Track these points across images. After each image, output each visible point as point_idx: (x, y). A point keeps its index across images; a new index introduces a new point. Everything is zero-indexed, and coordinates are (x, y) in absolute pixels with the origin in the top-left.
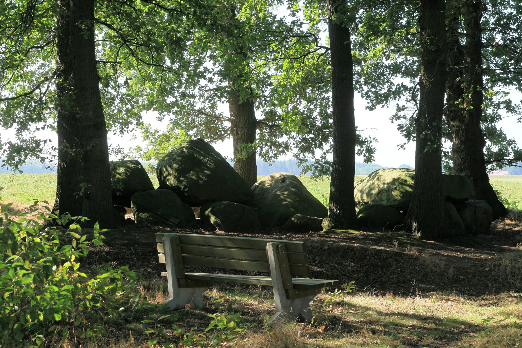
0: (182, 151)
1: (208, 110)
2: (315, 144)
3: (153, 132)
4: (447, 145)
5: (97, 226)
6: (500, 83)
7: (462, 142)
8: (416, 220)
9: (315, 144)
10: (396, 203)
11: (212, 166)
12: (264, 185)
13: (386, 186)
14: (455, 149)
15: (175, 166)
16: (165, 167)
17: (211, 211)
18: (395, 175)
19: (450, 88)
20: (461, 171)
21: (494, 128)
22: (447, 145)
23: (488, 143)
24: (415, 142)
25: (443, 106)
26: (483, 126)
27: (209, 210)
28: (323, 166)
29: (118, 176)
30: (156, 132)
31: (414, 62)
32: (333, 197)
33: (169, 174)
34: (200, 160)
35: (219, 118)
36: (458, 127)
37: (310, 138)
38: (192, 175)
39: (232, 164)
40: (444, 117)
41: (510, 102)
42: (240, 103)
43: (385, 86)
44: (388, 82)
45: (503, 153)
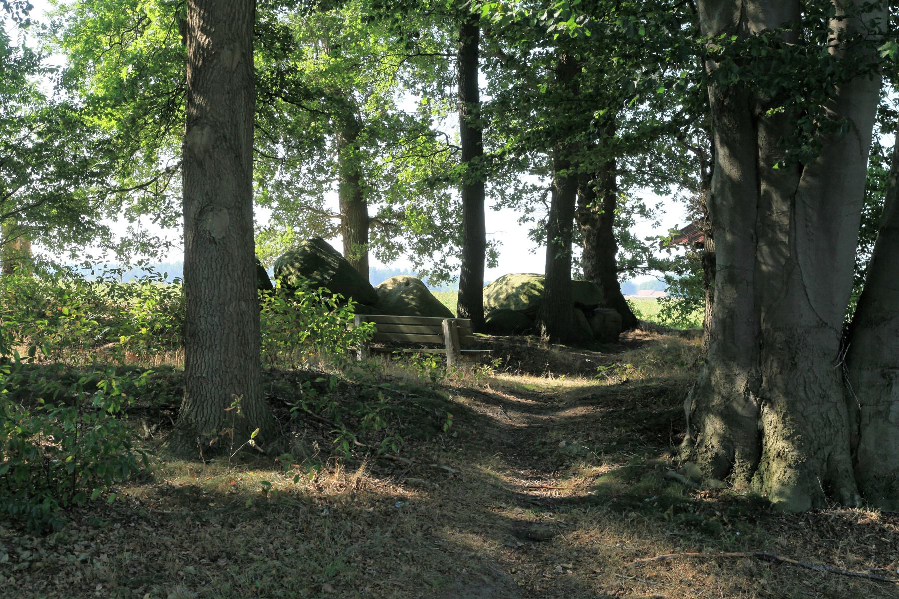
0: (304, 250)
1: (314, 204)
2: (433, 246)
4: (577, 251)
5: (350, 300)
6: (635, 185)
7: (593, 248)
8: (545, 324)
9: (433, 246)
10: (525, 308)
11: (336, 266)
14: (585, 256)
15: (297, 264)
16: (286, 266)
18: (525, 279)
19: (583, 190)
20: (592, 278)
21: (628, 234)
22: (577, 251)
23: (621, 249)
24: (546, 247)
25: (574, 207)
26: (616, 231)
28: (441, 271)
31: (544, 158)
32: (462, 300)
33: (290, 273)
34: (323, 259)
35: (326, 214)
36: (589, 231)
37: (428, 239)
40: (574, 220)
41: (644, 206)
43: (512, 184)
44: (515, 179)
45: (637, 260)
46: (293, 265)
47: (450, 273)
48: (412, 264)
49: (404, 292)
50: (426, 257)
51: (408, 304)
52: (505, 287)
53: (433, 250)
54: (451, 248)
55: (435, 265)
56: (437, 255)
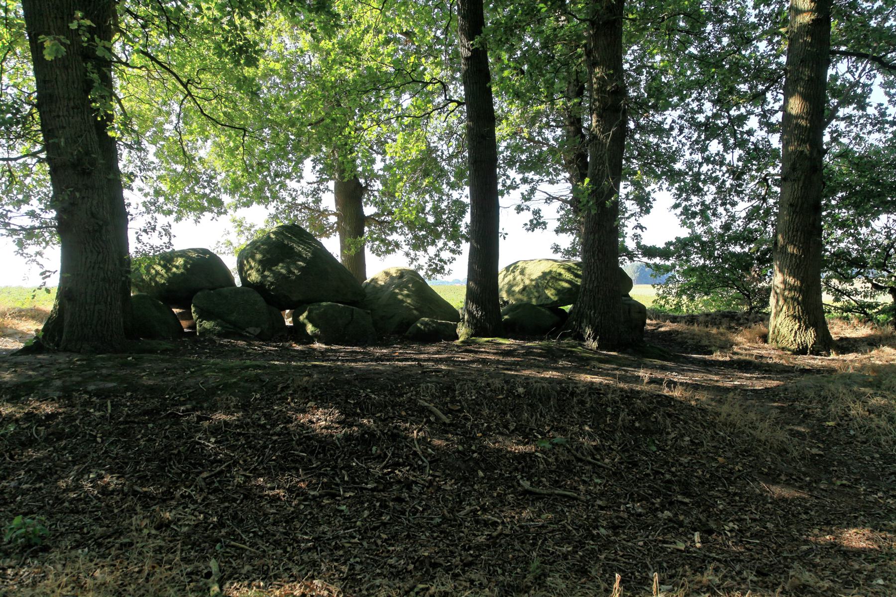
0: (269, 237)
1: (311, 204)
3: (248, 226)
12: (376, 282)
13: (534, 283)
17: (307, 318)
18: (546, 267)
27: (305, 314)
29: (174, 270)
30: (252, 226)
33: (251, 268)
35: (325, 213)
38: (281, 268)
39: (339, 260)
42: (346, 180)
46: (253, 258)
47: (445, 266)
48: (408, 260)
49: (397, 287)
50: (421, 253)
51: (402, 301)
52: (519, 278)
53: (428, 245)
54: (445, 244)
55: (430, 259)
56: (432, 250)
